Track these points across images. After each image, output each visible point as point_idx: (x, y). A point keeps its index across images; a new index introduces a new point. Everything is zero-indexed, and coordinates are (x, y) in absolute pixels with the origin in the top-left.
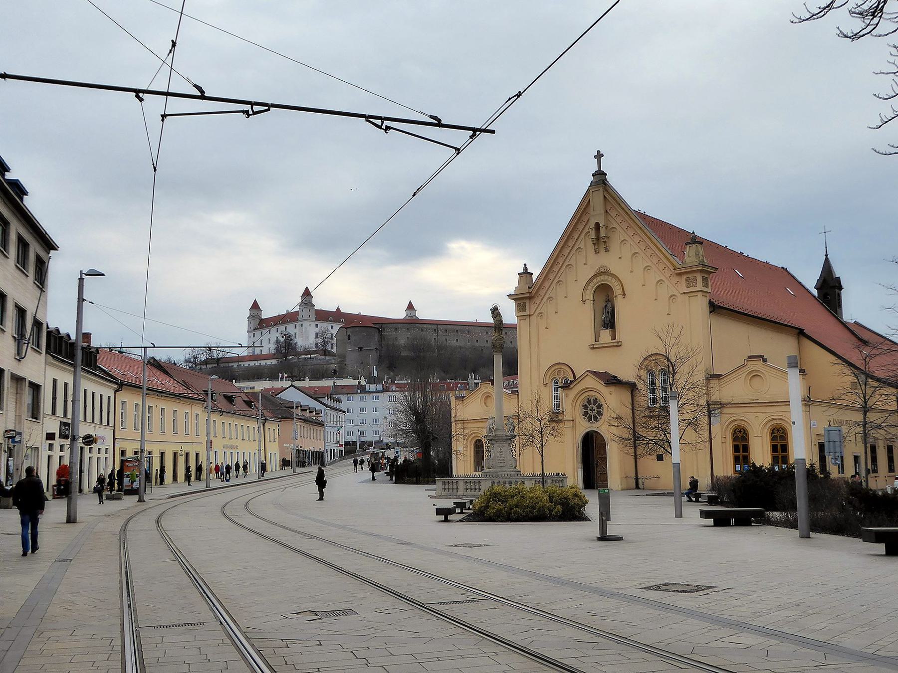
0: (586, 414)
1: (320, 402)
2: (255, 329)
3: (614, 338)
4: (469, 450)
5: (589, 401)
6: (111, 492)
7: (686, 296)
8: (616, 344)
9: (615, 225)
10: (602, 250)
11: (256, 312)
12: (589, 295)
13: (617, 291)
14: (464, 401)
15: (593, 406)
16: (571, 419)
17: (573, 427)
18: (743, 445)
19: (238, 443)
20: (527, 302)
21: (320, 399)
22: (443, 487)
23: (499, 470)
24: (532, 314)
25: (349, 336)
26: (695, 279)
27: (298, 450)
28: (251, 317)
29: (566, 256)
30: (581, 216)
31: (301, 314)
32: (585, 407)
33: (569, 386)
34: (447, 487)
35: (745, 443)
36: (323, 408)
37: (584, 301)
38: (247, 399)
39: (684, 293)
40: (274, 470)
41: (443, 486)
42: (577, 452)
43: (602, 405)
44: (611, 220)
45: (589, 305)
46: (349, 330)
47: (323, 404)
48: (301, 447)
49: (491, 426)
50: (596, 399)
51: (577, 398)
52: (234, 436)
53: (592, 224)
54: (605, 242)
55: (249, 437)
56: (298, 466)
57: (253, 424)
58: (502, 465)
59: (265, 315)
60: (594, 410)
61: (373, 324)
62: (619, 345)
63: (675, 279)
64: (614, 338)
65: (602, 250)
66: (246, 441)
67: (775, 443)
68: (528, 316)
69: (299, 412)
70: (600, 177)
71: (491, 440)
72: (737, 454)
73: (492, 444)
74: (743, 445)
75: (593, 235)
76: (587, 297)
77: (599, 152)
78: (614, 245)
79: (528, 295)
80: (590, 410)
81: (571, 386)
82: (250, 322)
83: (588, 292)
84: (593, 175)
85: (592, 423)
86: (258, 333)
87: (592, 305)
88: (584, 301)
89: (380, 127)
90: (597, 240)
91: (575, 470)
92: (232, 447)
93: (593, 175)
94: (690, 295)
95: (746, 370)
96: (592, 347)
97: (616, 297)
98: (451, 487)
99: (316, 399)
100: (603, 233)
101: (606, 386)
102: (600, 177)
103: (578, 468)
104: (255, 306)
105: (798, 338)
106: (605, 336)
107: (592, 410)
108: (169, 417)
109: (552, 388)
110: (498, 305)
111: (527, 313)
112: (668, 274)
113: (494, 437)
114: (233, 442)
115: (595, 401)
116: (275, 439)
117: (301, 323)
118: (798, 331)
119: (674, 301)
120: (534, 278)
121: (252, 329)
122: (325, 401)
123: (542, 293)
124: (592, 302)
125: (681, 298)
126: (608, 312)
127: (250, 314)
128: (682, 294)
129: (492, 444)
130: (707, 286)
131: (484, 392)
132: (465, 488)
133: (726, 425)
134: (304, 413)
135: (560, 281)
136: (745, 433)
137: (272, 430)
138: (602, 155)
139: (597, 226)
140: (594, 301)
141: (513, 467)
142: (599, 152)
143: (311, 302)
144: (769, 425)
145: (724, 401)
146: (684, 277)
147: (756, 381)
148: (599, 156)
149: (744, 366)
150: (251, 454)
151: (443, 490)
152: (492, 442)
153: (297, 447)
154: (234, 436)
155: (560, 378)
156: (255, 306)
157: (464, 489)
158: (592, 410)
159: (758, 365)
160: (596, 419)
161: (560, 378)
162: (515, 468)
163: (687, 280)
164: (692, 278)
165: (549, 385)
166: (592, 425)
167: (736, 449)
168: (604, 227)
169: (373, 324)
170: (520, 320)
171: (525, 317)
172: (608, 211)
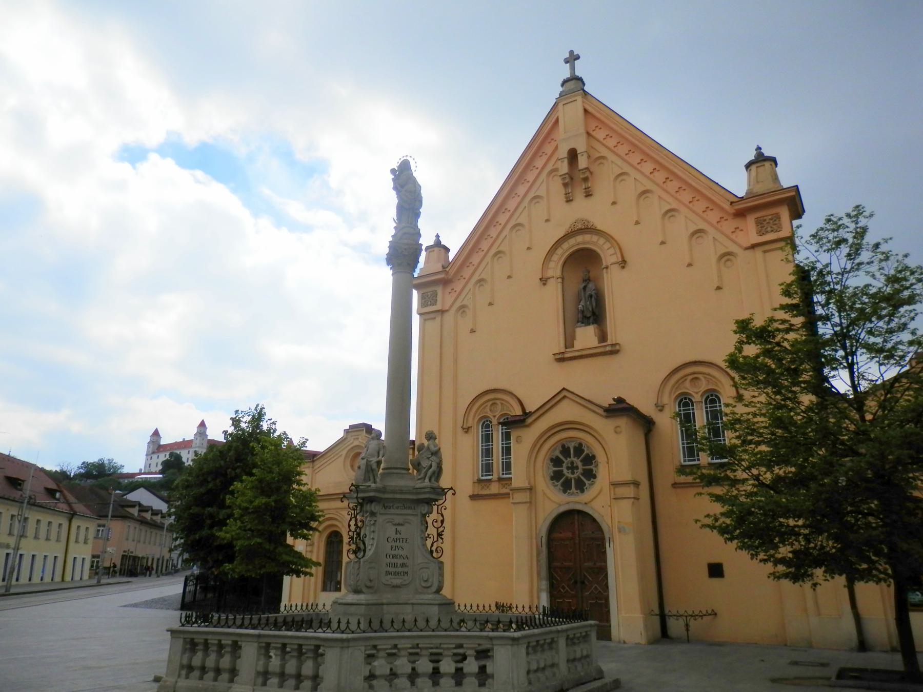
0: (556, 476)
2: (153, 453)
3: (603, 337)
4: (315, 550)
5: (565, 451)
7: (758, 253)
8: (608, 349)
9: (604, 152)
10: (579, 194)
11: (155, 438)
12: (555, 269)
13: (609, 256)
14: (316, 463)
15: (575, 460)
16: (526, 485)
17: (530, 502)
20: (439, 290)
22: (185, 662)
23: (387, 597)
24: (447, 308)
26: (778, 217)
27: (127, 556)
29: (502, 225)
30: (539, 148)
32: (556, 462)
33: (523, 421)
34: (197, 661)
37: (544, 281)
39: (753, 247)
40: (77, 577)
41: (186, 656)
42: (538, 554)
43: (594, 457)
44: (597, 146)
45: (554, 290)
48: (132, 552)
49: (374, 460)
50: (581, 445)
51: (545, 437)
53: (563, 152)
54: (586, 180)
58: (397, 581)
59: (163, 442)
60: (577, 468)
62: (614, 351)
63: (729, 225)
64: (603, 337)
65: (579, 194)
66: (42, 541)
68: (440, 313)
70: (574, 85)
71: (371, 500)
73: (373, 514)
75: (564, 168)
76: (550, 273)
77: (571, 52)
78: (603, 186)
79: (442, 276)
80: (568, 468)
81: (529, 420)
82: (149, 447)
83: (552, 265)
85: (573, 494)
86: (155, 456)
87: (560, 286)
88: (544, 281)
90: (569, 182)
91: (535, 595)
96: (560, 356)
97: (607, 268)
98: (211, 662)
100: (582, 162)
101: (607, 417)
102: (574, 85)
103: (539, 590)
104: (156, 433)
106: (586, 336)
107: (573, 468)
108: (43, 527)
109: (478, 432)
110: (408, 158)
111: (438, 307)
112: (714, 216)
113: (377, 490)
115: (579, 450)
119: (729, 263)
120: (451, 256)
121: (150, 452)
123: (467, 273)
124: (560, 280)
125: (743, 257)
126: (591, 296)
128: (747, 249)
129: (373, 514)
131: (351, 446)
132: (260, 668)
134: (155, 518)
135: (499, 252)
138: (578, 57)
139: (573, 155)
140: (563, 279)
141: (434, 589)
142: (571, 52)
143: (205, 432)
146: (751, 220)
148: (572, 58)
151: (184, 672)
152: (374, 507)
153: (125, 552)
155: (495, 416)
156: (156, 433)
157: (258, 673)
158: (573, 468)
160: (581, 487)
161: (495, 416)
162: (438, 591)
163: (759, 222)
164: (770, 217)
165: (474, 429)
166: (576, 499)
168: (585, 155)
170: (425, 320)
171: (432, 316)
172: (591, 132)
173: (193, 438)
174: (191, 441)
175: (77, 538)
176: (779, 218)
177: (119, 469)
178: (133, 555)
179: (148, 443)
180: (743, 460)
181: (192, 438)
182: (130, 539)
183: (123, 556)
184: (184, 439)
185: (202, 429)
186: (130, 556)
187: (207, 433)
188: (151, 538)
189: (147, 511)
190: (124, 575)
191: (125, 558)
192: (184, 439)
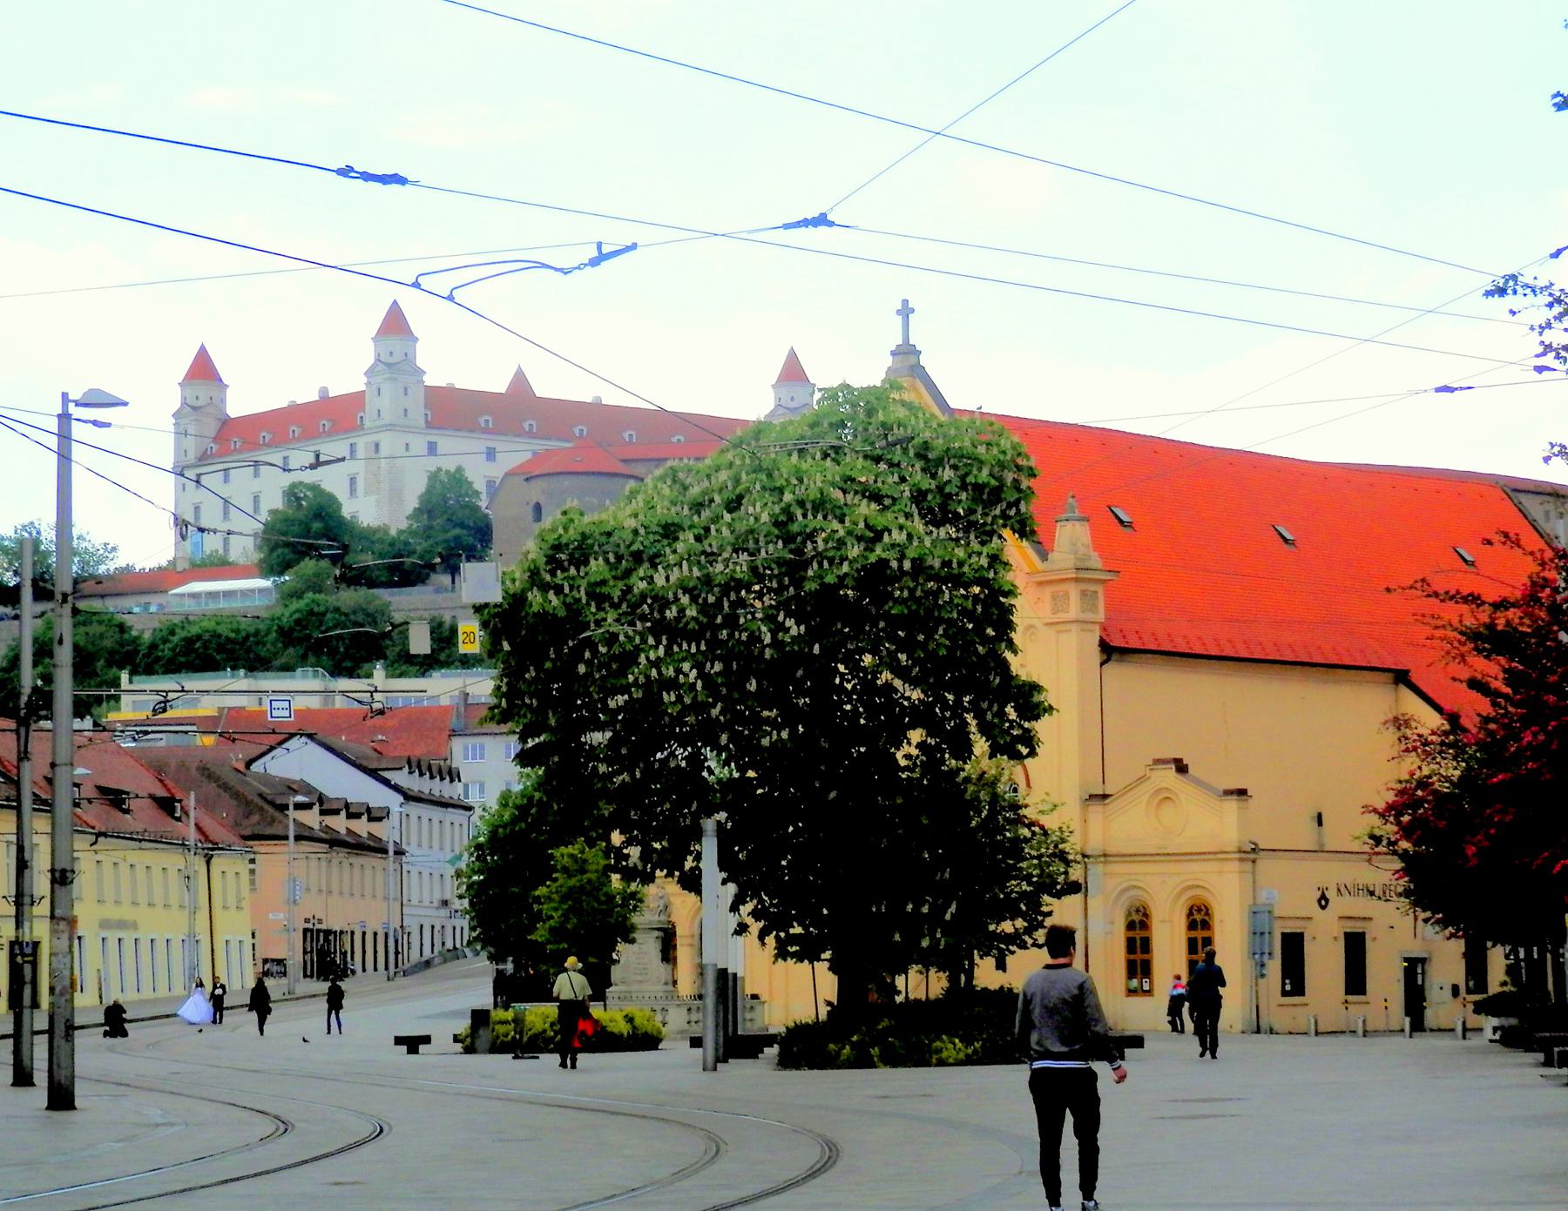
1: (386, 782)
6: (980, 816)
11: (203, 392)
18: (1141, 939)
19: (141, 914)
21: (386, 774)
23: (635, 987)
25: (538, 509)
26: (1066, 595)
27: (312, 930)
28: (189, 412)
31: (371, 404)
35: (1144, 934)
36: (393, 800)
38: (161, 793)
46: (539, 485)
47: (397, 788)
48: (320, 921)
52: (126, 896)
55: (166, 895)
56: (312, 976)
57: (173, 860)
58: (639, 978)
59: (238, 405)
61: (625, 461)
67: (1131, 934)
69: (312, 818)
72: (1145, 957)
74: (1141, 939)
77: (905, 302)
82: (181, 433)
84: (893, 353)
89: (229, 739)
92: (122, 925)
93: (893, 353)
94: (1059, 627)
95: (1147, 788)
99: (373, 773)
104: (203, 370)
105: (1396, 690)
114: (125, 912)
116: (239, 901)
117: (375, 437)
118: (1390, 675)
119: (1033, 637)
121: (192, 457)
122: (401, 778)
127: (184, 398)
130: (1094, 609)
133: (1114, 895)
134: (330, 821)
136: (1207, 914)
137: (230, 876)
138: (913, 311)
142: (905, 302)
144: (1184, 898)
145: (1111, 849)
146: (1049, 590)
147: (1168, 809)
148: (906, 311)
149: (1142, 779)
150: (172, 944)
153: (307, 921)
154: (126, 896)
156: (203, 370)
159: (1169, 775)
163: (1054, 597)
167: (1131, 945)
169: (625, 461)
173: (363, 388)
174: (355, 401)
175: (225, 900)
176: (1068, 597)
177: (99, 562)
178: (323, 927)
179: (176, 415)
180: (1466, 745)
181: (357, 384)
182: (314, 889)
183: (305, 931)
184: (324, 391)
185: (395, 344)
186: (319, 931)
187: (420, 362)
188: (351, 879)
189: (336, 812)
190: (312, 976)
191: (309, 935)
192: (324, 391)
